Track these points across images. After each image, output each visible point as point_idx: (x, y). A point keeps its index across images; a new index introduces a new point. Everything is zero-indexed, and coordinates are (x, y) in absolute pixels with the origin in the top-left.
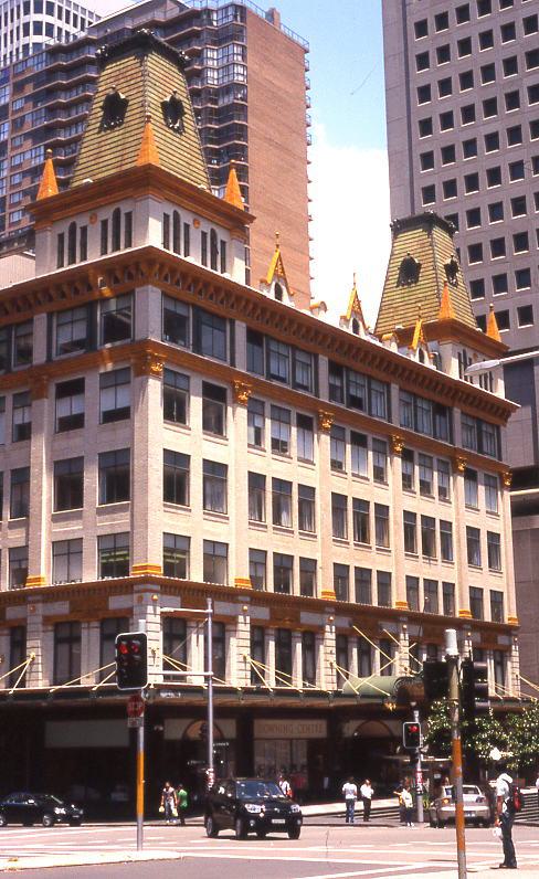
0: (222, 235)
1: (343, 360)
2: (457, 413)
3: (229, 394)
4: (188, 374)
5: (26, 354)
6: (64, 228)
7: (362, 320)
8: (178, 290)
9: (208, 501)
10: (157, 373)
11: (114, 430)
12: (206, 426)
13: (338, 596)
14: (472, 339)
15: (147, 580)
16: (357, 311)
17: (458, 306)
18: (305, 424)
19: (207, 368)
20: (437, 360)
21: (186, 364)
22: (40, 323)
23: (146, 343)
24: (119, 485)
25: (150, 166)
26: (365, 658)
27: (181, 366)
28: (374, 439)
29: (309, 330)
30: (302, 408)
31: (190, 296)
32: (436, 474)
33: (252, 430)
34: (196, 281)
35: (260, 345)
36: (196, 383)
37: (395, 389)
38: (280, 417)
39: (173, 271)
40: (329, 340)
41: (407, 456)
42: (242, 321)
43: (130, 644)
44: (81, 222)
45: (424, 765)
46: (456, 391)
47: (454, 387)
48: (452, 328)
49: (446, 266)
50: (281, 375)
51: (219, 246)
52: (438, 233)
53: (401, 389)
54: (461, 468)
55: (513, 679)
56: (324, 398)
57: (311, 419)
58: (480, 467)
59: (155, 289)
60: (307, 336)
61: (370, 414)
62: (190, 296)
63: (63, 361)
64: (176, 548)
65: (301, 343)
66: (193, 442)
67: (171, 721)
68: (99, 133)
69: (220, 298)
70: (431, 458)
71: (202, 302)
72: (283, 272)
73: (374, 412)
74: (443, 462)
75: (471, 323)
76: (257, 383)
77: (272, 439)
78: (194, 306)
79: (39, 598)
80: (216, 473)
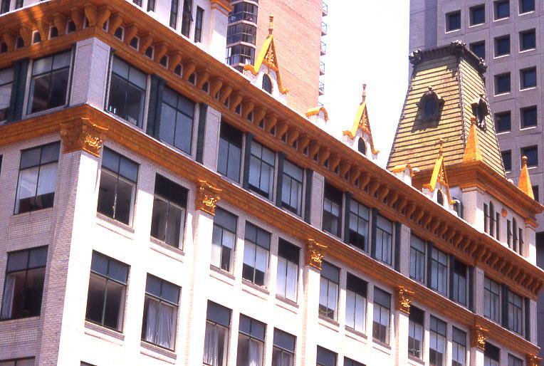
0: (520, 224)
1: (341, 183)
2: (479, 275)
3: (191, 197)
4: (138, 160)
7: (371, 141)
8: (134, 53)
9: (149, 331)
10: (317, 264)
11: (30, 222)
12: (156, 231)
14: (522, 205)
16: (365, 128)
17: (485, 148)
18: (289, 253)
19: (162, 157)
20: (459, 207)
21: (136, 147)
23: (83, 107)
27: (128, 149)
28: (376, 288)
29: (313, 143)
30: (285, 232)
31: (148, 63)
32: (450, 345)
33: (218, 251)
34: (158, 44)
35: (239, 145)
36: (147, 175)
37: (405, 232)
38: (257, 238)
39: (129, 26)
40: (387, 191)
41: (416, 317)
42: (218, 109)
47: (476, 239)
48: (479, 173)
49: (474, 106)
50: (293, 205)
52: (465, 67)
53: (413, 234)
54: (481, 341)
56: (316, 224)
57: (297, 249)
58: (504, 345)
59: (101, 43)
60: (303, 146)
61: (429, 286)
62: (148, 63)
65: (291, 152)
66: (135, 246)
68: (412, 131)
69: (189, 74)
70: (445, 324)
71: (166, 74)
72: (275, 62)
73: (378, 254)
74: (515, 358)
75: (497, 166)
76: (229, 190)
77: (245, 266)
78: (154, 76)
80: (163, 295)
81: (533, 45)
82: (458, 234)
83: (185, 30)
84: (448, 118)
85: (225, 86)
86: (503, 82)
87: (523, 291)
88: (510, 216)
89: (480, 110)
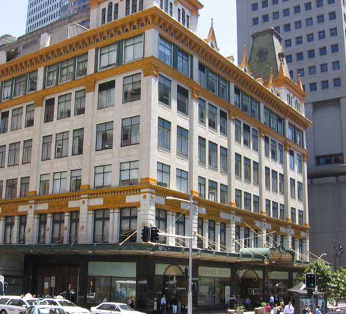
0: (187, 12)
2: (287, 122)
4: (170, 79)
5: (85, 71)
13: (237, 206)
22: (92, 53)
26: (43, 226)
46: (286, 111)
51: (186, 17)
63: (103, 72)
67: (159, 265)
79: (9, 230)
81: (340, 85)
82: (244, 80)
83: (184, 24)
85: (248, 82)
86: (288, 43)
87: (301, 129)
88: (296, 98)
89: (281, 55)
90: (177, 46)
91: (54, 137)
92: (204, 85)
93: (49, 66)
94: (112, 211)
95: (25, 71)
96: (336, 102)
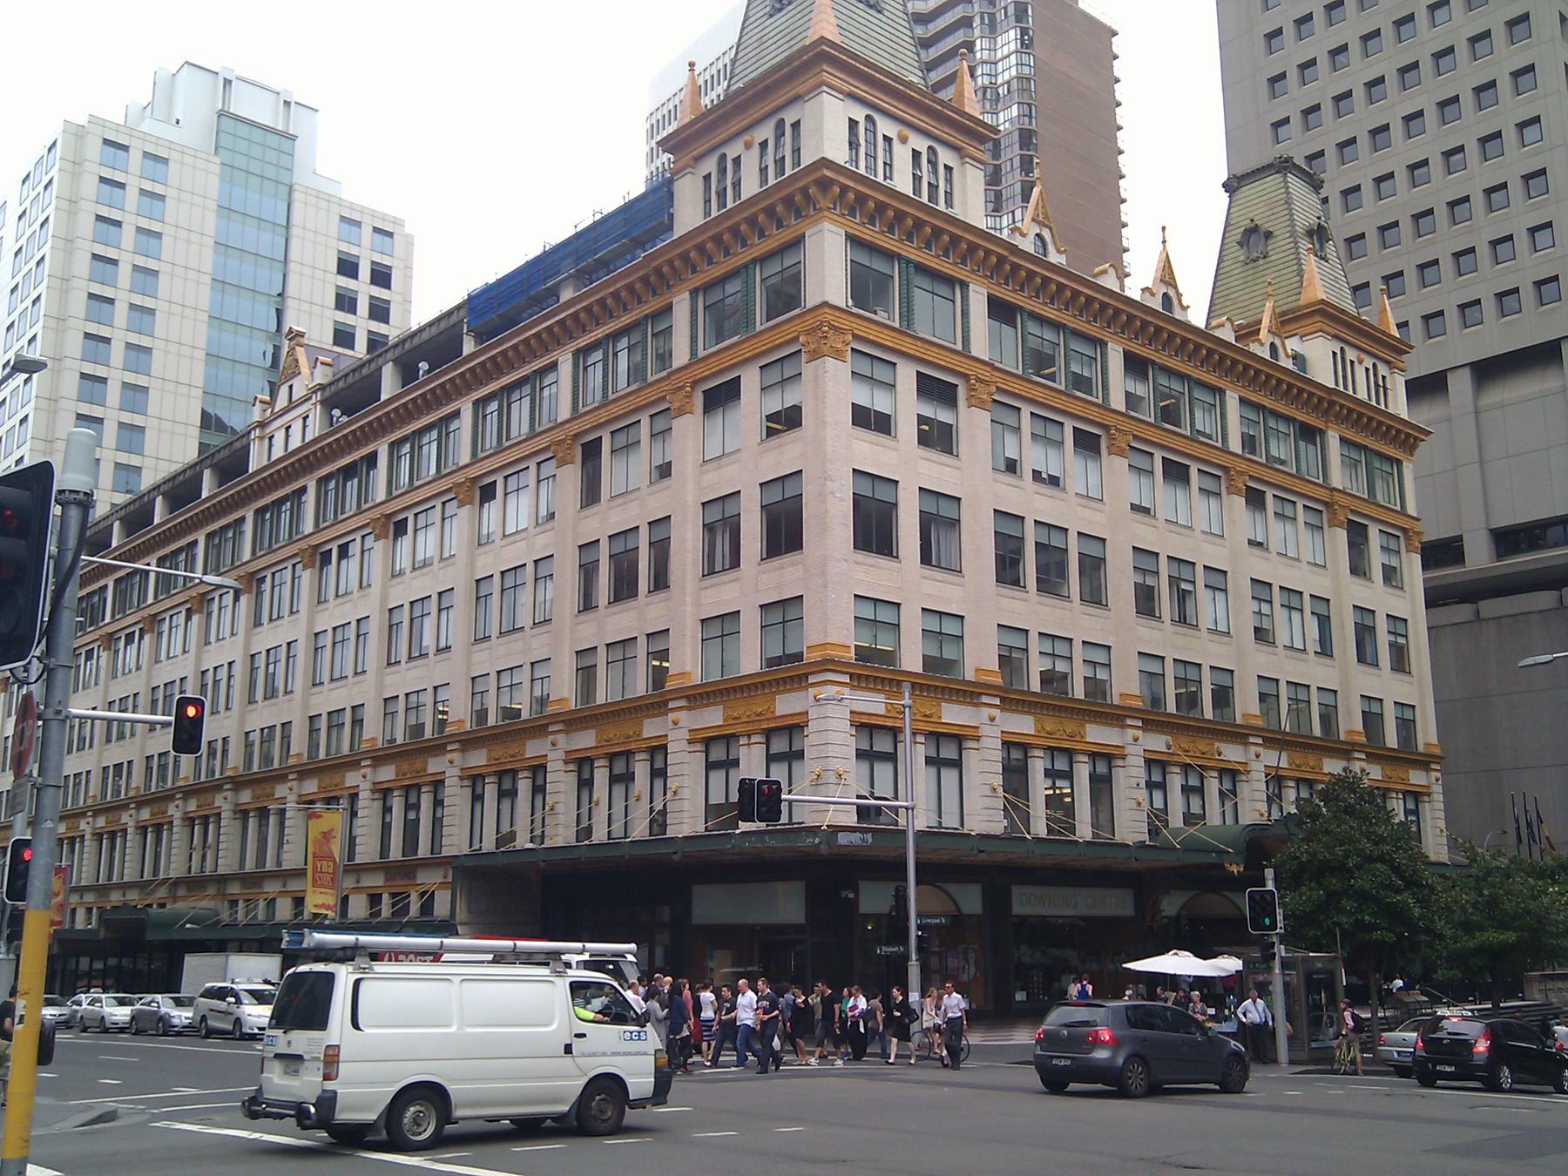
0: (1383, 370)
3: (962, 393)
6: (710, 165)
7: (1179, 295)
15: (827, 665)
17: (1322, 281)
18: (1087, 443)
24: (785, 532)
25: (823, 40)
43: (1263, 898)
44: (732, 151)
45: (1285, 965)
46: (1334, 405)
49: (1309, 233)
55: (1435, 836)
59: (834, 228)
64: (878, 614)
66: (909, 467)
75: (1349, 305)
79: (683, 703)
84: (1279, 247)
89: (1319, 234)
90: (909, 261)
91: (604, 544)
92: (1012, 362)
93: (707, 288)
94: (743, 741)
95: (743, 257)
96: (1544, 355)
